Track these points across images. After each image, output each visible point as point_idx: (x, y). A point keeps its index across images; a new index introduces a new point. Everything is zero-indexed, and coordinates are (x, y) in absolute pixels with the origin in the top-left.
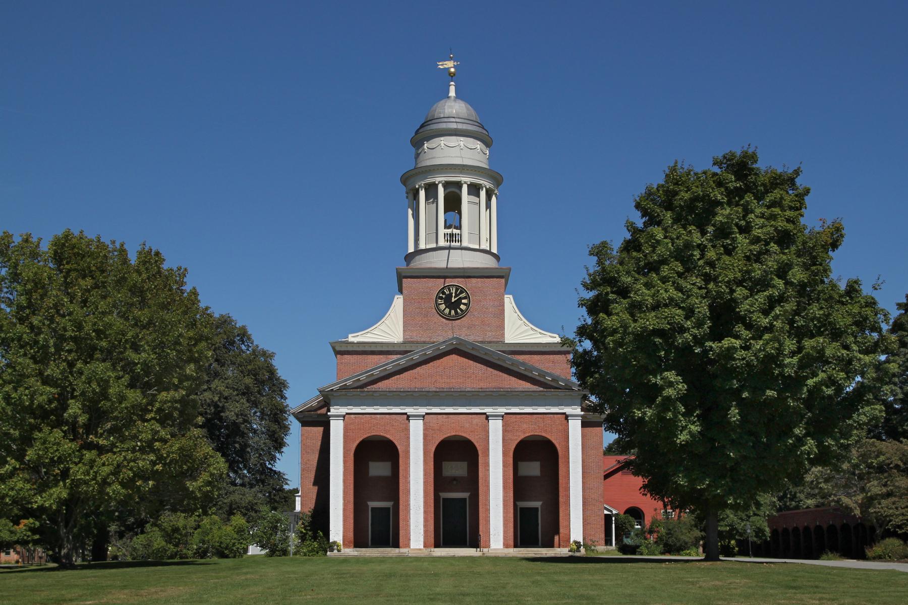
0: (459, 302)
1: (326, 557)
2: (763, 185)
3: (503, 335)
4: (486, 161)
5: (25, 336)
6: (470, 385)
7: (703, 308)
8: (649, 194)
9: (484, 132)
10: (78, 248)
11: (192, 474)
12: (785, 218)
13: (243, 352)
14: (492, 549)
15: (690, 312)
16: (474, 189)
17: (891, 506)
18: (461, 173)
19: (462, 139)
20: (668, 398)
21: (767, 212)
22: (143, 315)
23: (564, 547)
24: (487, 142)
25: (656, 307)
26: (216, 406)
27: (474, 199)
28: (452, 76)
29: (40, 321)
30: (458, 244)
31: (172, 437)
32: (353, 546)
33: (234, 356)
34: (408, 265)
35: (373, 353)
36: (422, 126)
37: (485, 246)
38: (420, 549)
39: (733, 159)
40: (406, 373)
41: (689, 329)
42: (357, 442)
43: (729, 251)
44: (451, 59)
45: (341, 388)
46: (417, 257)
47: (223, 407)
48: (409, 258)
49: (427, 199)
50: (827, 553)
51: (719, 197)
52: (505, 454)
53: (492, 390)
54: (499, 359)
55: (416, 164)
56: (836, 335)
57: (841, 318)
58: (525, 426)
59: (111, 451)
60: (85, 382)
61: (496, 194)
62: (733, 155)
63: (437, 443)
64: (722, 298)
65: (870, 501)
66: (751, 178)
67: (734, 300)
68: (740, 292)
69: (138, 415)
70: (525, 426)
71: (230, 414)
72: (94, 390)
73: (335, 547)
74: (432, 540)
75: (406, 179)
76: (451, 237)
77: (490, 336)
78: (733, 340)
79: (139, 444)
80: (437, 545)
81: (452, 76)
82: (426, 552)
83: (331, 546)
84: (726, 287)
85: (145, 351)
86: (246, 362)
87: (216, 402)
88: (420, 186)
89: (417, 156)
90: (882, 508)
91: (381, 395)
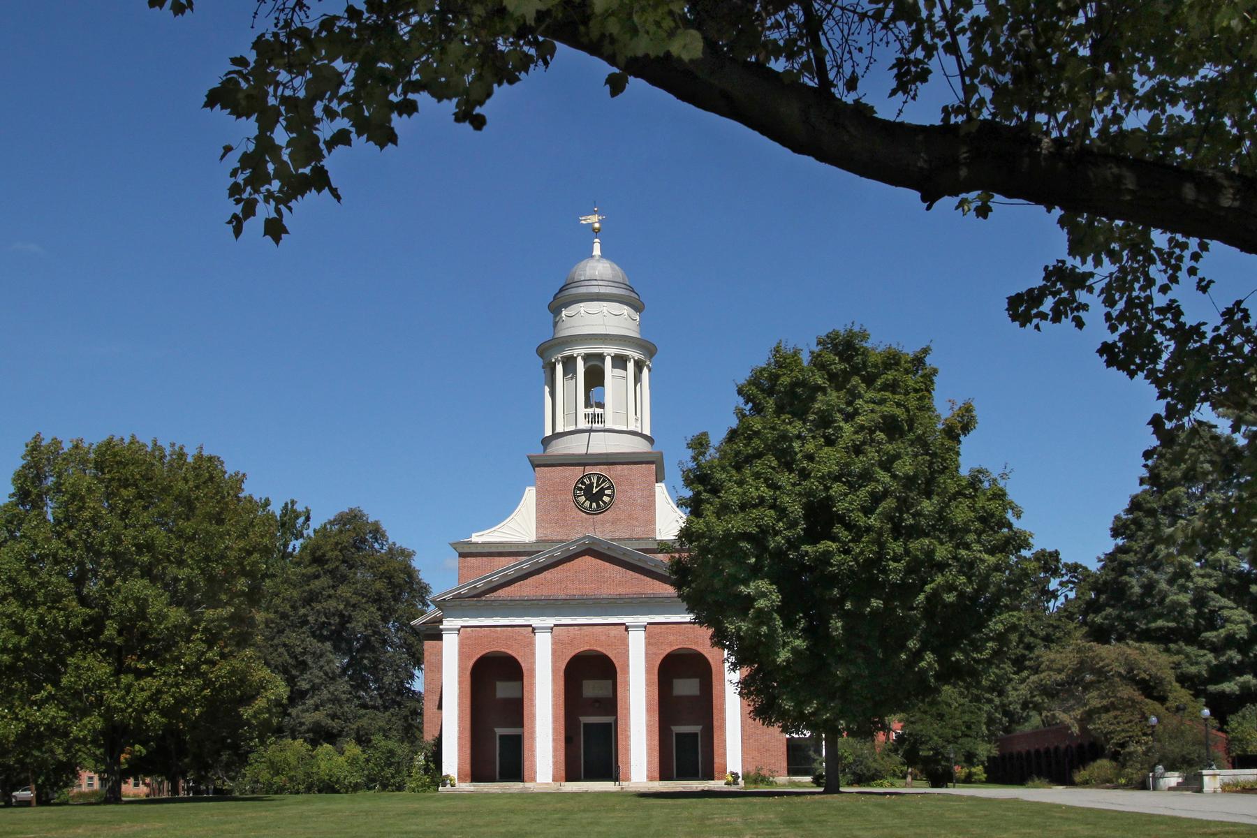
0: (601, 493)
1: (436, 794)
2: (875, 366)
3: (654, 530)
4: (637, 329)
5: (60, 551)
6: (607, 591)
7: (796, 510)
8: (755, 381)
9: (633, 295)
10: (120, 456)
11: (247, 700)
12: (895, 402)
13: (377, 552)
15: (782, 512)
16: (620, 361)
17: (1112, 721)
18: (603, 343)
19: (605, 304)
20: (760, 611)
21: (878, 396)
22: (188, 527)
23: (719, 779)
24: (637, 307)
25: (743, 507)
26: (341, 615)
27: (619, 372)
28: (596, 232)
29: (76, 536)
30: (600, 426)
31: (221, 659)
32: (470, 780)
33: (364, 557)
34: (545, 449)
35: (501, 554)
36: (561, 290)
38: (548, 784)
39: (836, 339)
40: (531, 578)
41: (781, 531)
42: (475, 659)
43: (830, 442)
44: (595, 212)
45: (454, 598)
46: (554, 442)
47: (350, 616)
48: (546, 442)
49: (565, 374)
50: (1033, 781)
51: (820, 381)
53: (631, 596)
54: (639, 560)
55: (554, 334)
56: (956, 533)
57: (960, 513)
58: (672, 638)
59: (150, 675)
60: (122, 602)
61: (648, 366)
62: (836, 334)
63: (568, 659)
64: (814, 496)
65: (1089, 715)
66: (858, 359)
67: (829, 498)
68: (837, 488)
69: (182, 637)
70: (672, 638)
71: (358, 625)
72: (130, 610)
73: (448, 781)
74: (563, 773)
75: (543, 351)
76: (594, 418)
77: (638, 532)
78: (830, 543)
79: (182, 667)
80: (570, 778)
82: (555, 787)
83: (444, 781)
84: (820, 483)
85: (188, 566)
86: (379, 563)
87: (341, 611)
88: (556, 360)
89: (555, 324)
90: (1102, 723)
91: (501, 605)
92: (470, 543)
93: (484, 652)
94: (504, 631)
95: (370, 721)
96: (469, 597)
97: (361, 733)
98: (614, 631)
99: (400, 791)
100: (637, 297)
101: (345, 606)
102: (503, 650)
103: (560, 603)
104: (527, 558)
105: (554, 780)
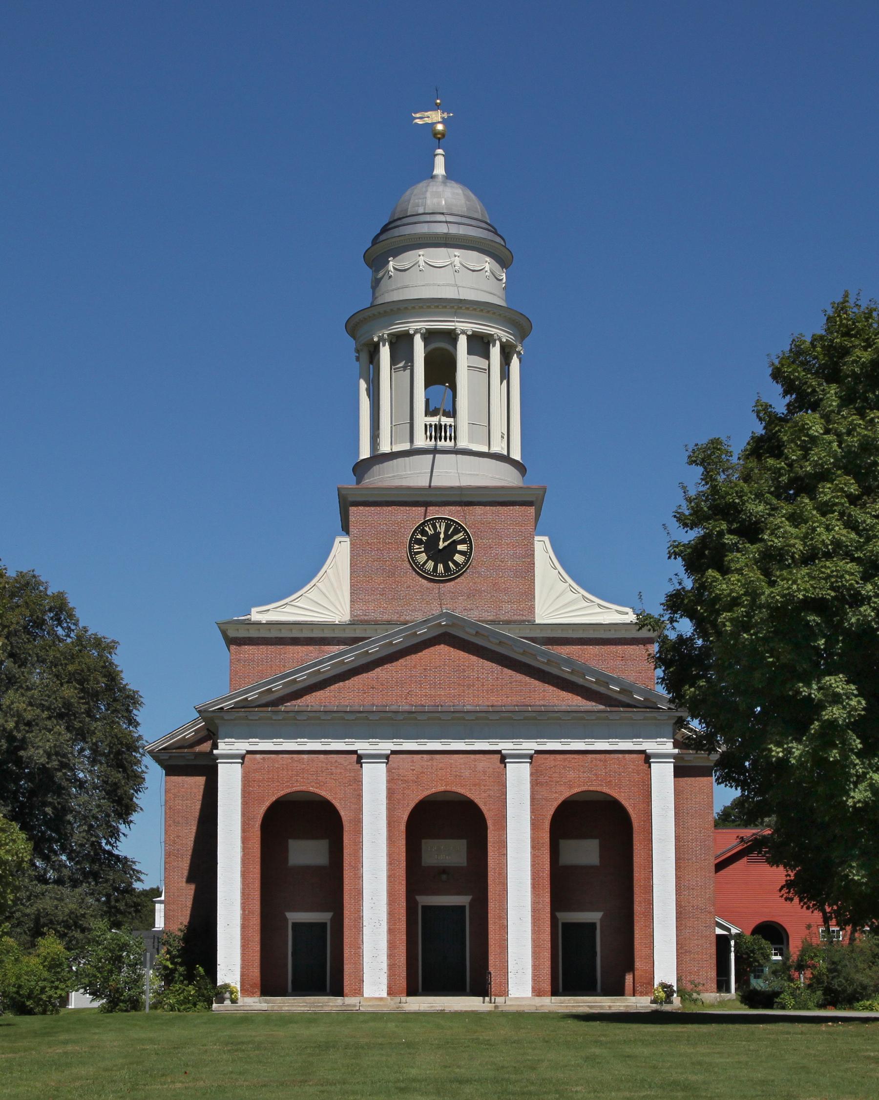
0: (451, 549)
3: (532, 609)
4: (502, 294)
6: (472, 701)
9: (498, 240)
14: (512, 999)
18: (456, 314)
19: (457, 252)
23: (642, 994)
24: (504, 261)
25: (809, 559)
28: (439, 138)
30: (449, 444)
32: (259, 993)
34: (359, 482)
35: (295, 641)
36: (385, 229)
37: (499, 447)
38: (381, 999)
40: (356, 678)
41: (869, 598)
42: (268, 804)
44: (437, 107)
45: (238, 707)
46: (376, 468)
48: (361, 468)
49: (394, 361)
52: (535, 825)
53: (511, 708)
55: (374, 297)
58: (571, 775)
61: (519, 353)
70: (571, 775)
74: (403, 983)
75: (354, 326)
77: (507, 611)
81: (439, 139)
82: (392, 1004)
83: (222, 994)
86: (65, 658)
87: (11, 731)
88: (381, 339)
89: (376, 283)
91: (309, 719)
92: (250, 623)
93: (282, 793)
94: (313, 760)
95: (56, 902)
96: (259, 706)
97: (42, 920)
98: (483, 763)
99: (136, 1010)
100: (502, 243)
101: (17, 723)
102: (311, 789)
103: (401, 717)
104: (342, 648)
105: (390, 993)
